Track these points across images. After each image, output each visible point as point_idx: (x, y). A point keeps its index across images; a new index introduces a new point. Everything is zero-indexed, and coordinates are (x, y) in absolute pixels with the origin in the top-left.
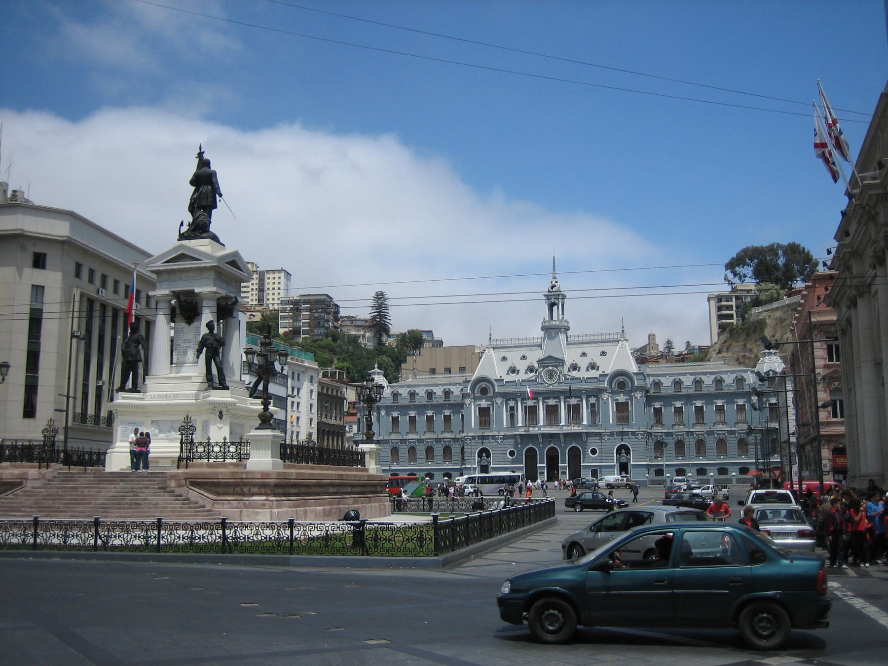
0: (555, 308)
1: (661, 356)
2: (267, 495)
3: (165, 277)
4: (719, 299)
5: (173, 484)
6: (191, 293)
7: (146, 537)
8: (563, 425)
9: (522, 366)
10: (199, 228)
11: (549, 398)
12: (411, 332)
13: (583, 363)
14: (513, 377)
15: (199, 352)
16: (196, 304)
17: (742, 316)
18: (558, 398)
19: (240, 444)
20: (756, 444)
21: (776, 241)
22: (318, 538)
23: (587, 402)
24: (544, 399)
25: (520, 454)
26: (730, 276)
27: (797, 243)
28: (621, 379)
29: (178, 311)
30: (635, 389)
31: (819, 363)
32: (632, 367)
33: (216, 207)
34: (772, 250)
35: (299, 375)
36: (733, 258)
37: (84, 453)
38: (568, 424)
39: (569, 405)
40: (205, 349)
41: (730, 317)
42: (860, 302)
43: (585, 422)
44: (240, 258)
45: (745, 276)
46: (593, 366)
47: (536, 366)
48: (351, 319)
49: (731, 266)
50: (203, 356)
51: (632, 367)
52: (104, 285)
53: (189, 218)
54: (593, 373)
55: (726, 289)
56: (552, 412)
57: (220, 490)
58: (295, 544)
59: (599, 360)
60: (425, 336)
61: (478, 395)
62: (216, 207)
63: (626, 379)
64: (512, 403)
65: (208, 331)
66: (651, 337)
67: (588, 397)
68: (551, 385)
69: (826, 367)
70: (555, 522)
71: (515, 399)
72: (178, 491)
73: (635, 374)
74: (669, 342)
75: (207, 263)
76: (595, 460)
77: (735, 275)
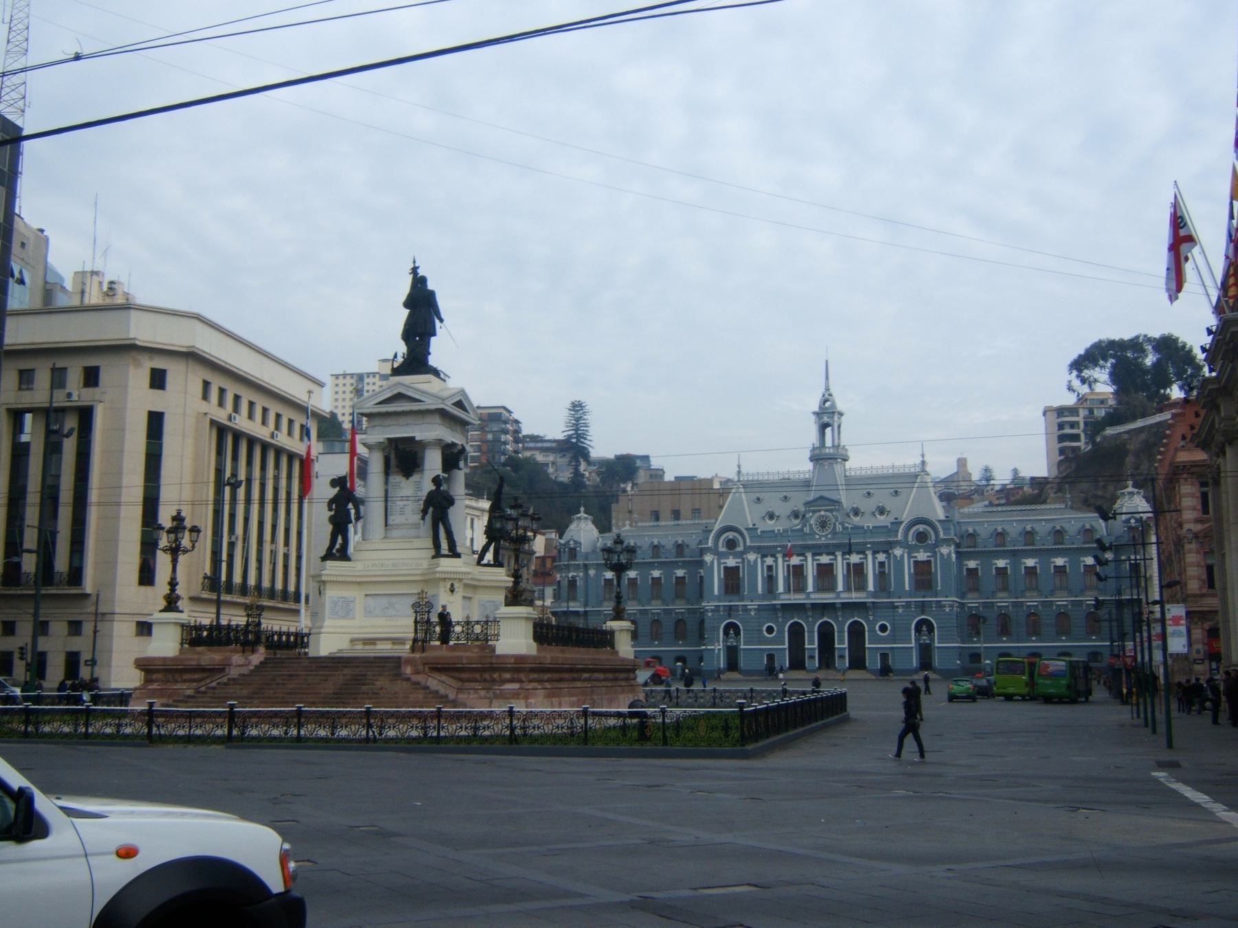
0: (828, 430)
1: (976, 491)
2: (520, 681)
3: (377, 421)
4: (1061, 411)
5: (408, 670)
6: (412, 439)
7: (425, 728)
8: (842, 593)
9: (783, 510)
10: (416, 361)
11: (820, 554)
12: (620, 458)
13: (867, 505)
14: (770, 524)
15: (425, 512)
16: (416, 453)
17: (1091, 438)
18: (833, 554)
19: (487, 622)
20: (1110, 620)
21: (1143, 332)
22: (615, 727)
23: (874, 559)
24: (814, 555)
25: (781, 631)
26: (1076, 383)
27: (1176, 334)
28: (921, 528)
29: (393, 462)
30: (939, 542)
31: (1188, 515)
32: (938, 511)
33: (434, 334)
34: (1136, 345)
35: (472, 520)
36: (1080, 356)
37: (273, 634)
38: (848, 589)
39: (848, 564)
40: (431, 509)
41: (1076, 438)
42: (1228, 450)
43: (871, 587)
44: (467, 397)
45: (1096, 381)
46: (882, 511)
47: (802, 509)
48: (535, 438)
49: (1080, 364)
50: (429, 517)
51: (938, 511)
52: (236, 409)
53: (402, 348)
54: (882, 520)
55: (1070, 400)
56: (825, 572)
57: (465, 676)
58: (590, 734)
59: (889, 503)
60: (639, 463)
61: (722, 549)
62: (434, 334)
63: (932, 533)
64: (769, 561)
65: (434, 488)
66: (962, 463)
67: (875, 553)
68: (822, 538)
69: (1197, 521)
70: (847, 720)
71: (773, 556)
72: (416, 678)
73: (940, 521)
74: (987, 470)
75: (431, 404)
76: (884, 640)
77: (1083, 381)
